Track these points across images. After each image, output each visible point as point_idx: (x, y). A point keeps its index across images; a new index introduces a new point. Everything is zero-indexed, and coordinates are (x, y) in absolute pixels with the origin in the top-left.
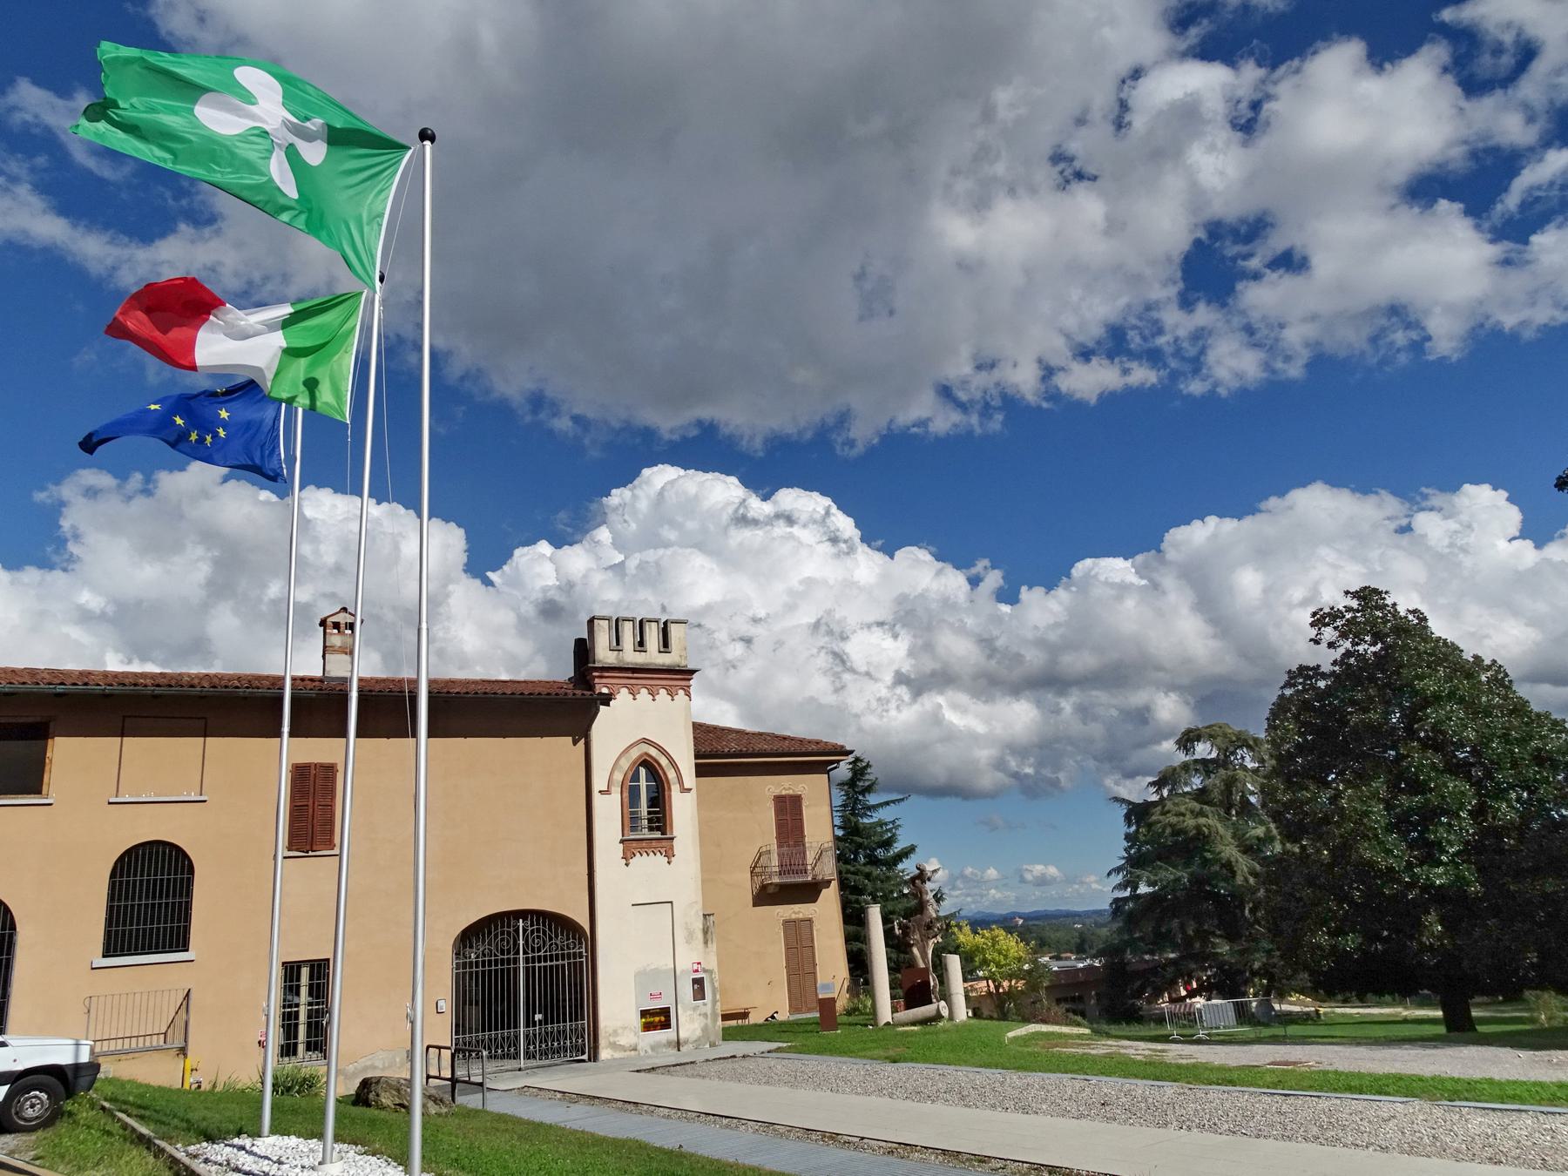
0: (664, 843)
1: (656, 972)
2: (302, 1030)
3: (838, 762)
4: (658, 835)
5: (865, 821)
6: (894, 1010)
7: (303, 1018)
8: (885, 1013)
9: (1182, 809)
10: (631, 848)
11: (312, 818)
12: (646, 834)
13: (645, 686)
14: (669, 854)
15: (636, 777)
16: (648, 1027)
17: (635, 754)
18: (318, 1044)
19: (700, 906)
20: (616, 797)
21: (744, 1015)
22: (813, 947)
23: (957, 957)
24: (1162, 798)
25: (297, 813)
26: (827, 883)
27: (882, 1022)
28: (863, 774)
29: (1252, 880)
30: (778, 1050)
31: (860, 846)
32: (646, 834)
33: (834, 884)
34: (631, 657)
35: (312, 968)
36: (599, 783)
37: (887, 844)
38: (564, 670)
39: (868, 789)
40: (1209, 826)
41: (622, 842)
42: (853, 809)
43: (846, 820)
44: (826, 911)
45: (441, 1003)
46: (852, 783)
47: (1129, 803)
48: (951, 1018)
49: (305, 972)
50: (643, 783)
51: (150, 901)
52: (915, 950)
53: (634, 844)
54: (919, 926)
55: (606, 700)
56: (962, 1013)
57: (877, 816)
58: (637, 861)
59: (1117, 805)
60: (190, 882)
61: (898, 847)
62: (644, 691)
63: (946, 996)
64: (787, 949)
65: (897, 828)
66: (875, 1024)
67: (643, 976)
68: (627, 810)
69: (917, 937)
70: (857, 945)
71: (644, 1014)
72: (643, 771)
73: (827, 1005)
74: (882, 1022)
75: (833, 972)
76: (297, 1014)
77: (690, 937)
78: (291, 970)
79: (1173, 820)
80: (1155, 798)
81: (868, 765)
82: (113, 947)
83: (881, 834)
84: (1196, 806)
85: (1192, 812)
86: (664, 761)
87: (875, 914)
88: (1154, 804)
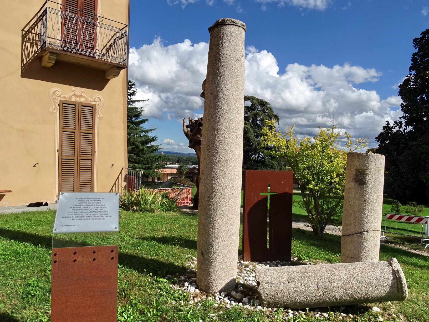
22: (93, 134)
40: (248, 128)
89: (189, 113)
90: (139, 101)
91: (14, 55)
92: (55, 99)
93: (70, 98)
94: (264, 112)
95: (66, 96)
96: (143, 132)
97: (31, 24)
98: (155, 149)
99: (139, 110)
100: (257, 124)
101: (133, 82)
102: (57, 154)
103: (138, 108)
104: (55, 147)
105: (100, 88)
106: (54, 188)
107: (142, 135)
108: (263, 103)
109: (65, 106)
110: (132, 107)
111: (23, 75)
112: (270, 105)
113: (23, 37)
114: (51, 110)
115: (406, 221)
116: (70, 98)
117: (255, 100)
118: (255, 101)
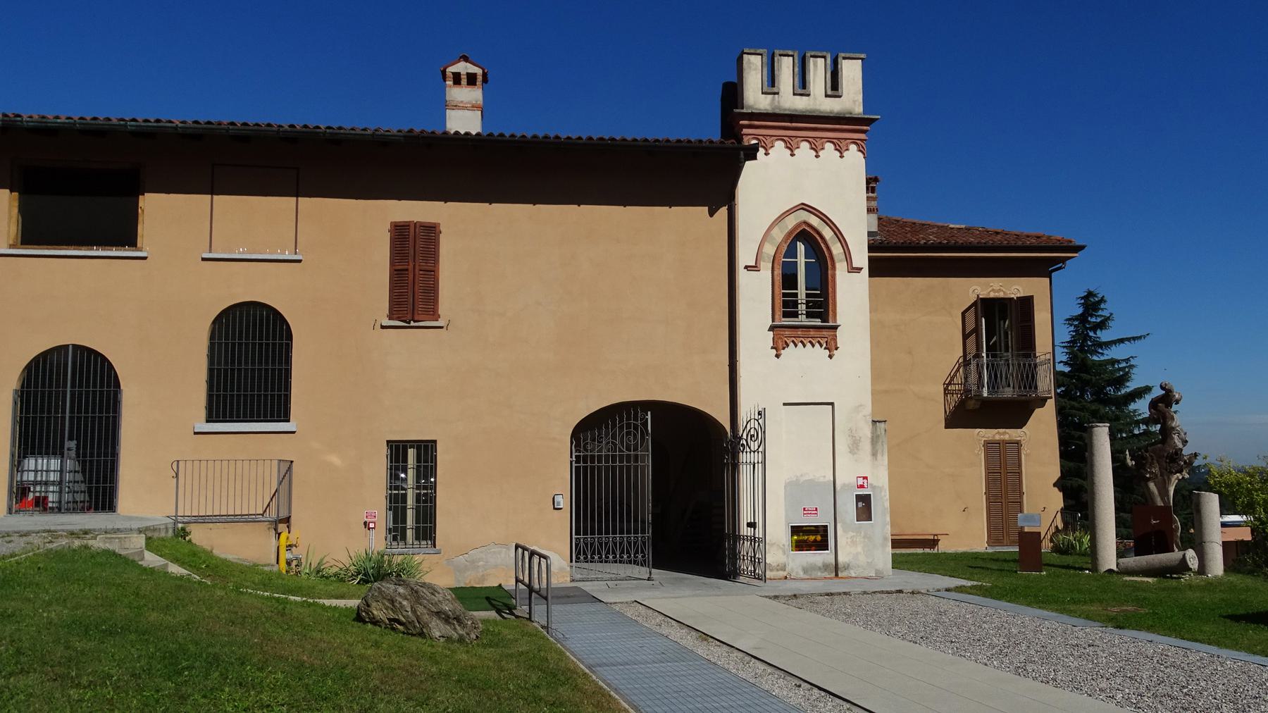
0: (825, 333)
1: (812, 485)
2: (410, 515)
3: (1064, 260)
4: (818, 322)
6: (1120, 554)
7: (410, 501)
8: (1109, 557)
10: (782, 337)
11: (413, 289)
12: (803, 320)
13: (806, 139)
14: (831, 347)
15: (791, 252)
16: (800, 546)
17: (791, 222)
18: (427, 532)
19: (868, 409)
20: (765, 275)
21: (933, 543)
22: (1020, 474)
23: (1216, 497)
25: (399, 276)
26: (1042, 402)
27: (1249, 538)
28: (1097, 309)
30: (959, 589)
31: (1088, 383)
32: (803, 320)
33: (1051, 404)
34: (789, 101)
35: (418, 449)
36: (745, 256)
37: (1121, 381)
38: (709, 130)
39: (1102, 325)
41: (772, 328)
44: (1040, 436)
45: (558, 499)
46: (1082, 319)
48: (1202, 569)
49: (411, 453)
50: (801, 260)
51: (250, 366)
52: (1152, 486)
53: (787, 332)
55: (751, 154)
56: (1217, 566)
57: (1110, 354)
58: (790, 352)
60: (289, 347)
61: (1131, 386)
62: (805, 146)
64: (988, 473)
65: (1132, 367)
66: (1094, 568)
67: (795, 488)
68: (780, 291)
69: (1156, 470)
70: (1077, 482)
71: (795, 530)
72: (801, 247)
73: (1030, 541)
74: (1249, 538)
75: (1043, 504)
76: (405, 496)
77: (854, 447)
78: (397, 450)
81: (1102, 300)
82: (216, 411)
83: (1112, 372)
86: (827, 233)
87: (1102, 437)
89: (1246, 524)
90: (1121, 341)
91: (938, 412)
96: (1137, 423)
99: (1124, 365)
101: (1100, 296)
103: (1118, 362)
105: (1020, 424)
107: (1136, 432)
109: (988, 445)
110: (1102, 358)
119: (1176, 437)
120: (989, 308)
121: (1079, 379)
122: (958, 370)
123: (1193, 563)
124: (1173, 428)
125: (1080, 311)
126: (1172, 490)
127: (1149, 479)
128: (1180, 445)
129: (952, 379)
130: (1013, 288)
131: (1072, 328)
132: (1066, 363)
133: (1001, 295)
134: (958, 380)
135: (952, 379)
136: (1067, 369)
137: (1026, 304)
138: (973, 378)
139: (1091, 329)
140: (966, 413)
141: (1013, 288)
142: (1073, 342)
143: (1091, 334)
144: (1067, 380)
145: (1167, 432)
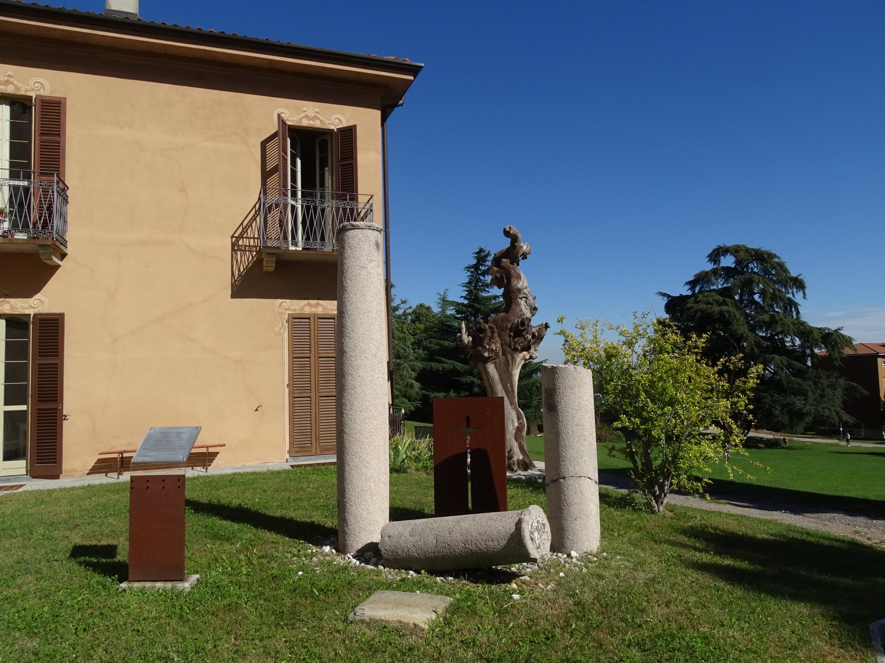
5: (484, 294)
9: (711, 300)
24: (694, 295)
28: (485, 261)
29: (756, 350)
40: (729, 313)
42: (476, 286)
43: (470, 292)
46: (476, 267)
47: (669, 296)
52: (491, 368)
54: (501, 329)
59: (661, 297)
63: (550, 489)
69: (496, 346)
79: (703, 306)
80: (689, 293)
84: (721, 299)
85: (717, 302)
88: (687, 297)
91: (221, 271)
92: (282, 314)
93: (302, 309)
94: (769, 273)
95: (297, 307)
97: (245, 223)
98: (791, 304)
100: (754, 302)
102: (287, 390)
104: (283, 382)
106: (284, 440)
108: (760, 256)
109: (296, 321)
110: (488, 295)
111: (234, 296)
112: (778, 258)
113: (233, 245)
114: (277, 329)
115: (215, 454)
116: (302, 309)
117: (742, 253)
118: (742, 254)
119: (522, 302)
120: (308, 143)
121: (473, 307)
122: (254, 219)
123: (538, 542)
124: (519, 290)
125: (475, 262)
126: (516, 373)
127: (487, 360)
128: (527, 313)
129: (245, 230)
130: (329, 116)
131: (469, 274)
132: (465, 298)
133: (317, 124)
134: (253, 232)
135: (245, 230)
136: (466, 302)
137: (348, 134)
138: (274, 231)
139: (481, 274)
140: (268, 273)
141: (329, 116)
142: (470, 283)
143: (482, 278)
144: (464, 309)
145: (511, 296)
